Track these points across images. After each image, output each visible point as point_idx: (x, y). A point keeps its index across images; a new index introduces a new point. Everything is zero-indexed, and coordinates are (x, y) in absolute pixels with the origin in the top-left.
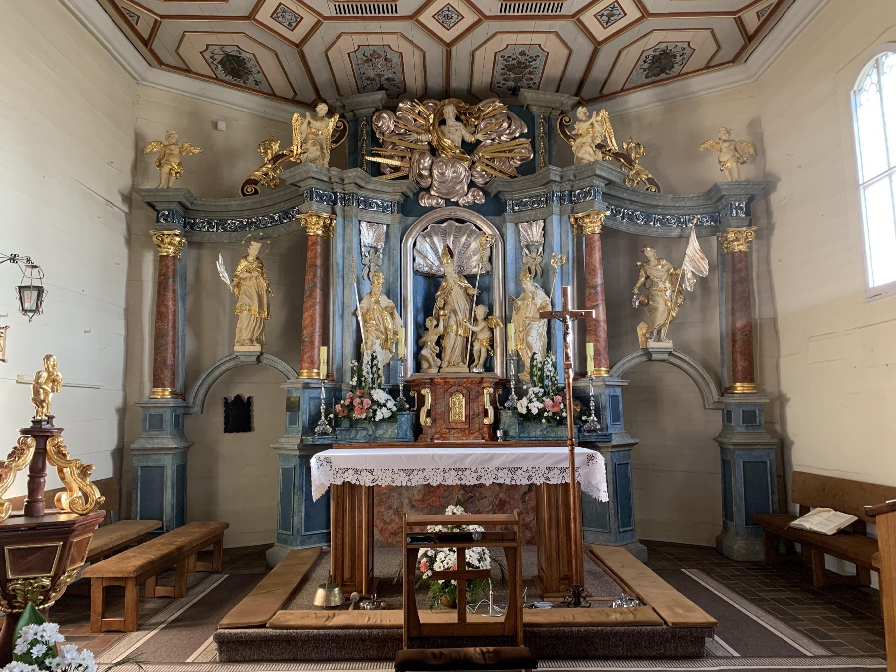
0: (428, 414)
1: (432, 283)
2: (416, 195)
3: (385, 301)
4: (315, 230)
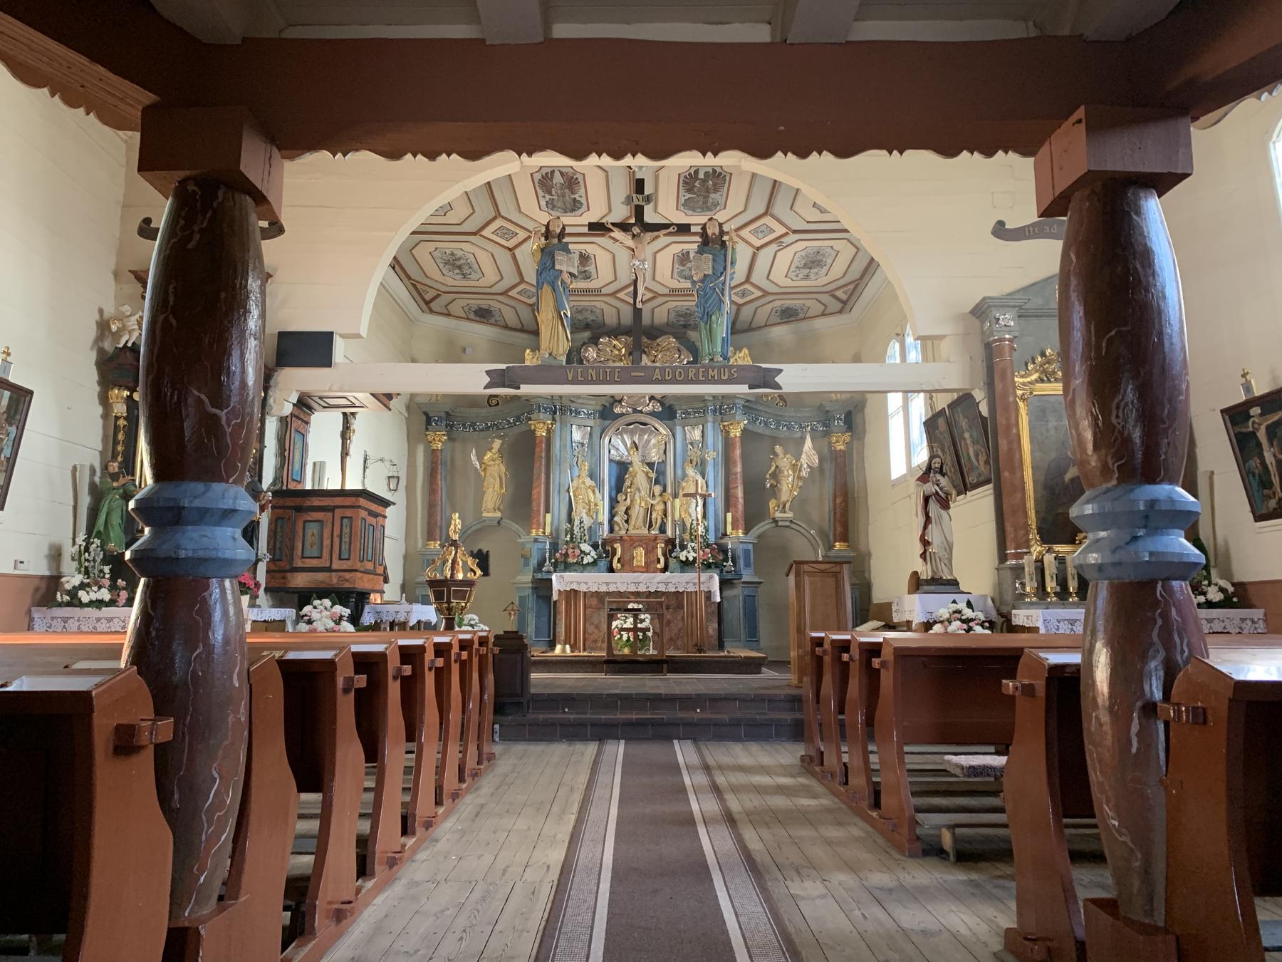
0: (619, 561)
1: (622, 468)
2: (612, 405)
3: (589, 482)
4: (541, 432)
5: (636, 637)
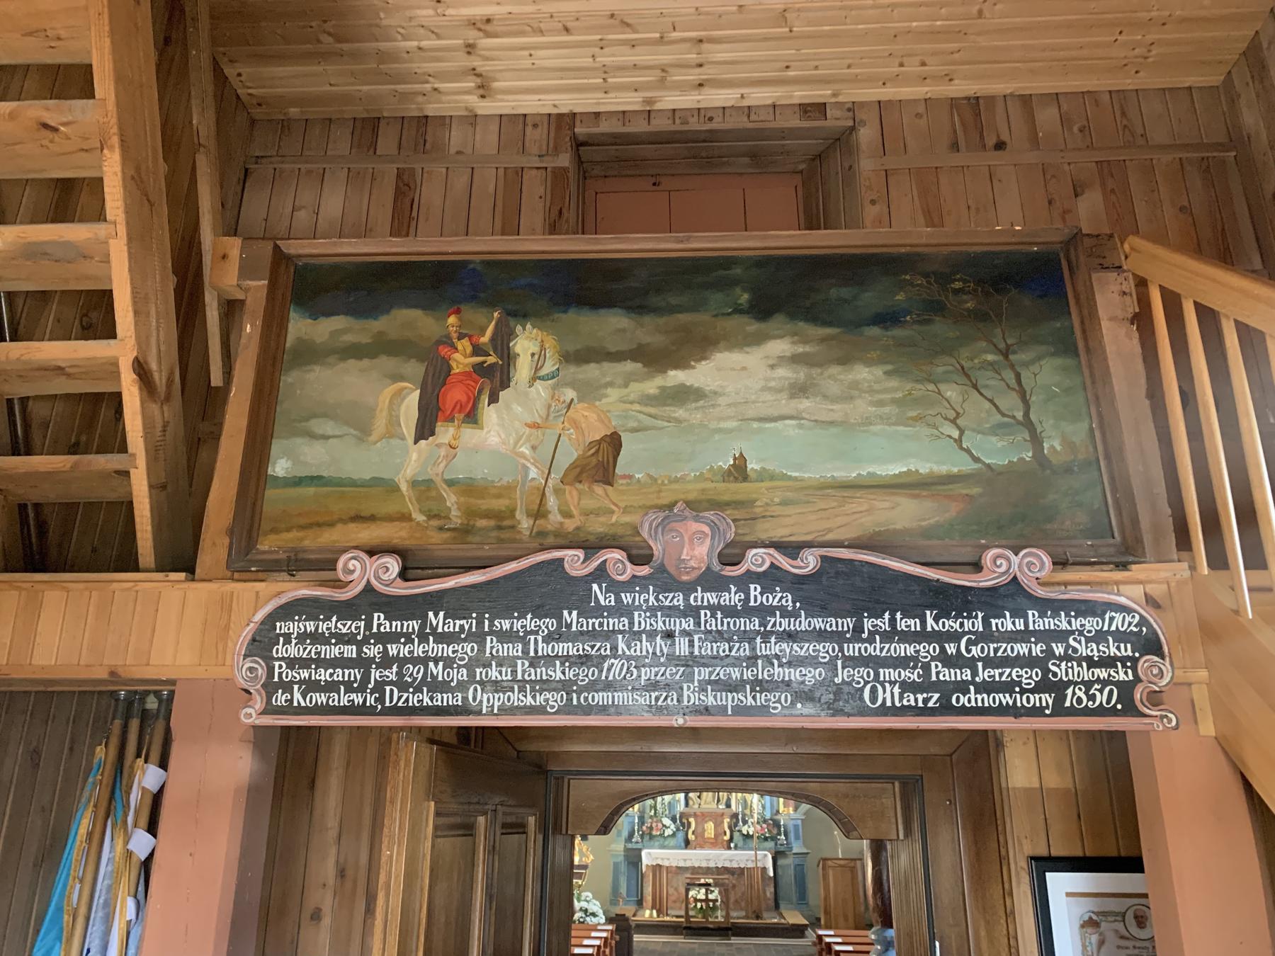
5: (708, 906)
